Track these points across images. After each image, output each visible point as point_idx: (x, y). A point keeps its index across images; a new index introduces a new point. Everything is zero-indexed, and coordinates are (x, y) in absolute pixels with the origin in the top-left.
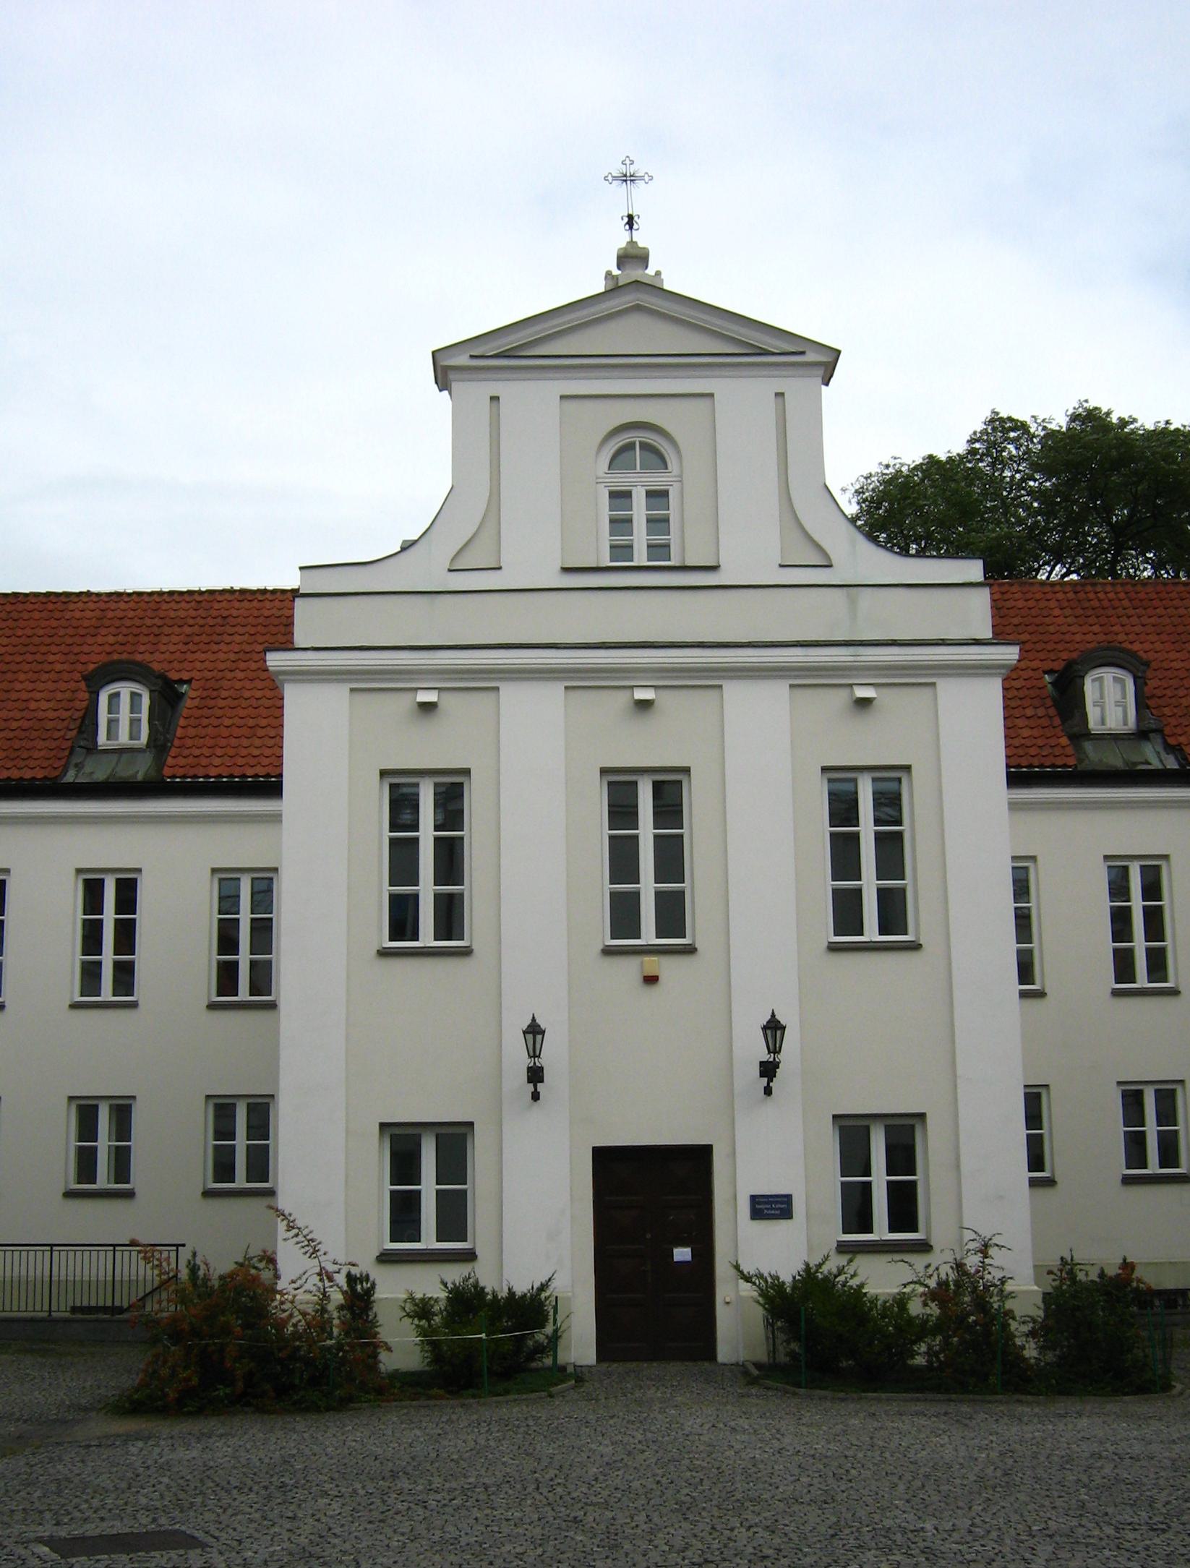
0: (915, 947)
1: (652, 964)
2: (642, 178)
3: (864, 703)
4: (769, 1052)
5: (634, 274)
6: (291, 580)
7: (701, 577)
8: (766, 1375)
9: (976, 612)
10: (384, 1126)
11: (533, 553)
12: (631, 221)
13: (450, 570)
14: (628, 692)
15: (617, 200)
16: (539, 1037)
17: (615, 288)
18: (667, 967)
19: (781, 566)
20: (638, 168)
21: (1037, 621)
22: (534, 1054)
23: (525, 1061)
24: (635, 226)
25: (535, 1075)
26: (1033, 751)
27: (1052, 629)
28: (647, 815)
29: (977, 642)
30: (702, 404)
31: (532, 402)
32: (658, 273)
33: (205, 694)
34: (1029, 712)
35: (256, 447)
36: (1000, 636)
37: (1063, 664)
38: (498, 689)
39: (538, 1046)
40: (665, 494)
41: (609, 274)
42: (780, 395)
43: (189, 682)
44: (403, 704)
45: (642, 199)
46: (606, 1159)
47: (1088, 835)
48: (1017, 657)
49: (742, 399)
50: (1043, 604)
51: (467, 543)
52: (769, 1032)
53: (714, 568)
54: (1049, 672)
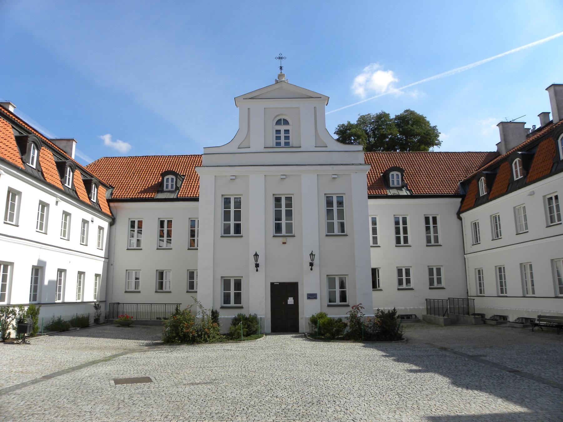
1: (283, 240)
12: (281, 68)
15: (278, 63)
18: (289, 240)
20: (283, 56)
22: (256, 261)
25: (257, 266)
31: (258, 106)
40: (288, 131)
45: (284, 63)
47: (384, 211)
49: (306, 106)
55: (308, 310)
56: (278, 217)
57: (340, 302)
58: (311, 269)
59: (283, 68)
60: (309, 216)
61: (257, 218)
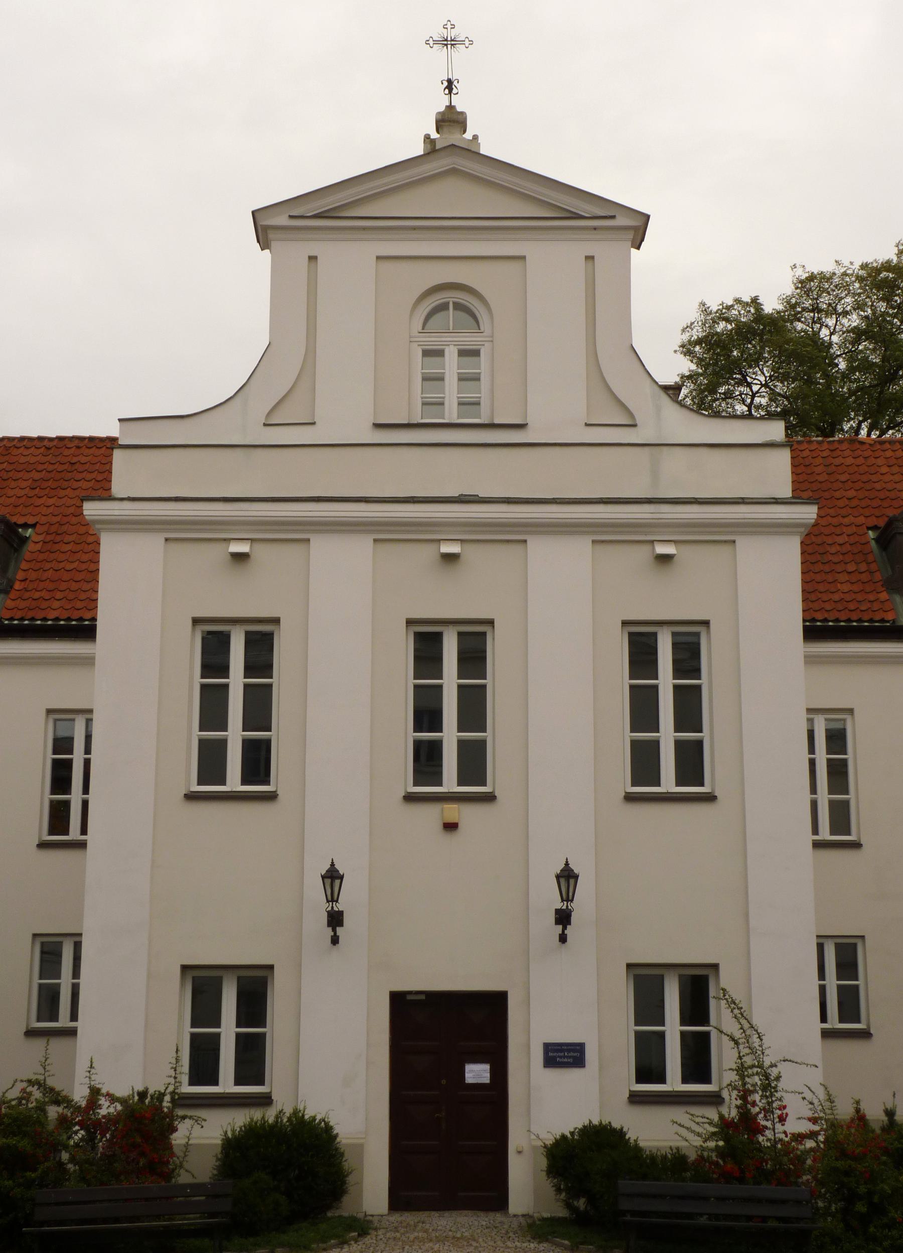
0: (710, 798)
1: (452, 811)
2: (462, 42)
3: (665, 559)
4: (563, 900)
5: (453, 138)
6: (111, 429)
7: (505, 434)
8: (539, 1229)
9: (776, 472)
10: (185, 968)
11: (346, 408)
13: (265, 425)
14: (433, 546)
16: (337, 882)
17: (432, 148)
18: (469, 816)
19: (586, 425)
20: (459, 32)
21: (864, 478)
22: (332, 898)
23: (323, 907)
24: (455, 91)
25: (335, 919)
26: (852, 606)
27: (878, 486)
28: (450, 666)
29: (776, 501)
30: (512, 267)
31: (350, 262)
32: (475, 137)
33: (49, 538)
34: (851, 567)
35: (96, 302)
36: (799, 496)
37: (886, 519)
38: (309, 540)
39: (571, 894)
40: (476, 353)
41: (427, 137)
42: (590, 258)
43: (33, 526)
44: (216, 554)
45: (461, 62)
46: (402, 1005)
48: (815, 516)
49: (554, 261)
50: (872, 461)
51: (282, 394)
52: (562, 881)
53: (521, 426)
54: (874, 528)
55: (546, 1109)
56: (427, 715)
57: (685, 1080)
58: (563, 939)
59: (458, 87)
60: (559, 706)
61: (342, 707)
